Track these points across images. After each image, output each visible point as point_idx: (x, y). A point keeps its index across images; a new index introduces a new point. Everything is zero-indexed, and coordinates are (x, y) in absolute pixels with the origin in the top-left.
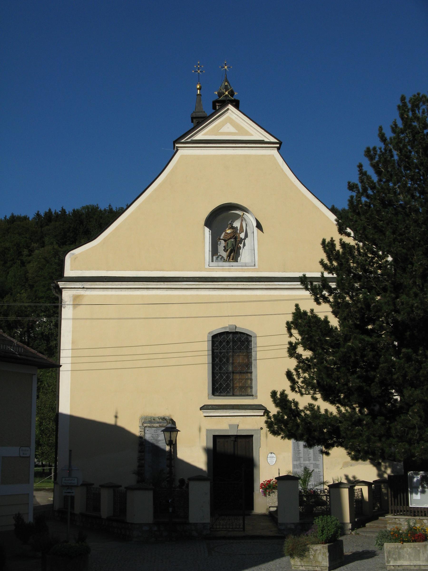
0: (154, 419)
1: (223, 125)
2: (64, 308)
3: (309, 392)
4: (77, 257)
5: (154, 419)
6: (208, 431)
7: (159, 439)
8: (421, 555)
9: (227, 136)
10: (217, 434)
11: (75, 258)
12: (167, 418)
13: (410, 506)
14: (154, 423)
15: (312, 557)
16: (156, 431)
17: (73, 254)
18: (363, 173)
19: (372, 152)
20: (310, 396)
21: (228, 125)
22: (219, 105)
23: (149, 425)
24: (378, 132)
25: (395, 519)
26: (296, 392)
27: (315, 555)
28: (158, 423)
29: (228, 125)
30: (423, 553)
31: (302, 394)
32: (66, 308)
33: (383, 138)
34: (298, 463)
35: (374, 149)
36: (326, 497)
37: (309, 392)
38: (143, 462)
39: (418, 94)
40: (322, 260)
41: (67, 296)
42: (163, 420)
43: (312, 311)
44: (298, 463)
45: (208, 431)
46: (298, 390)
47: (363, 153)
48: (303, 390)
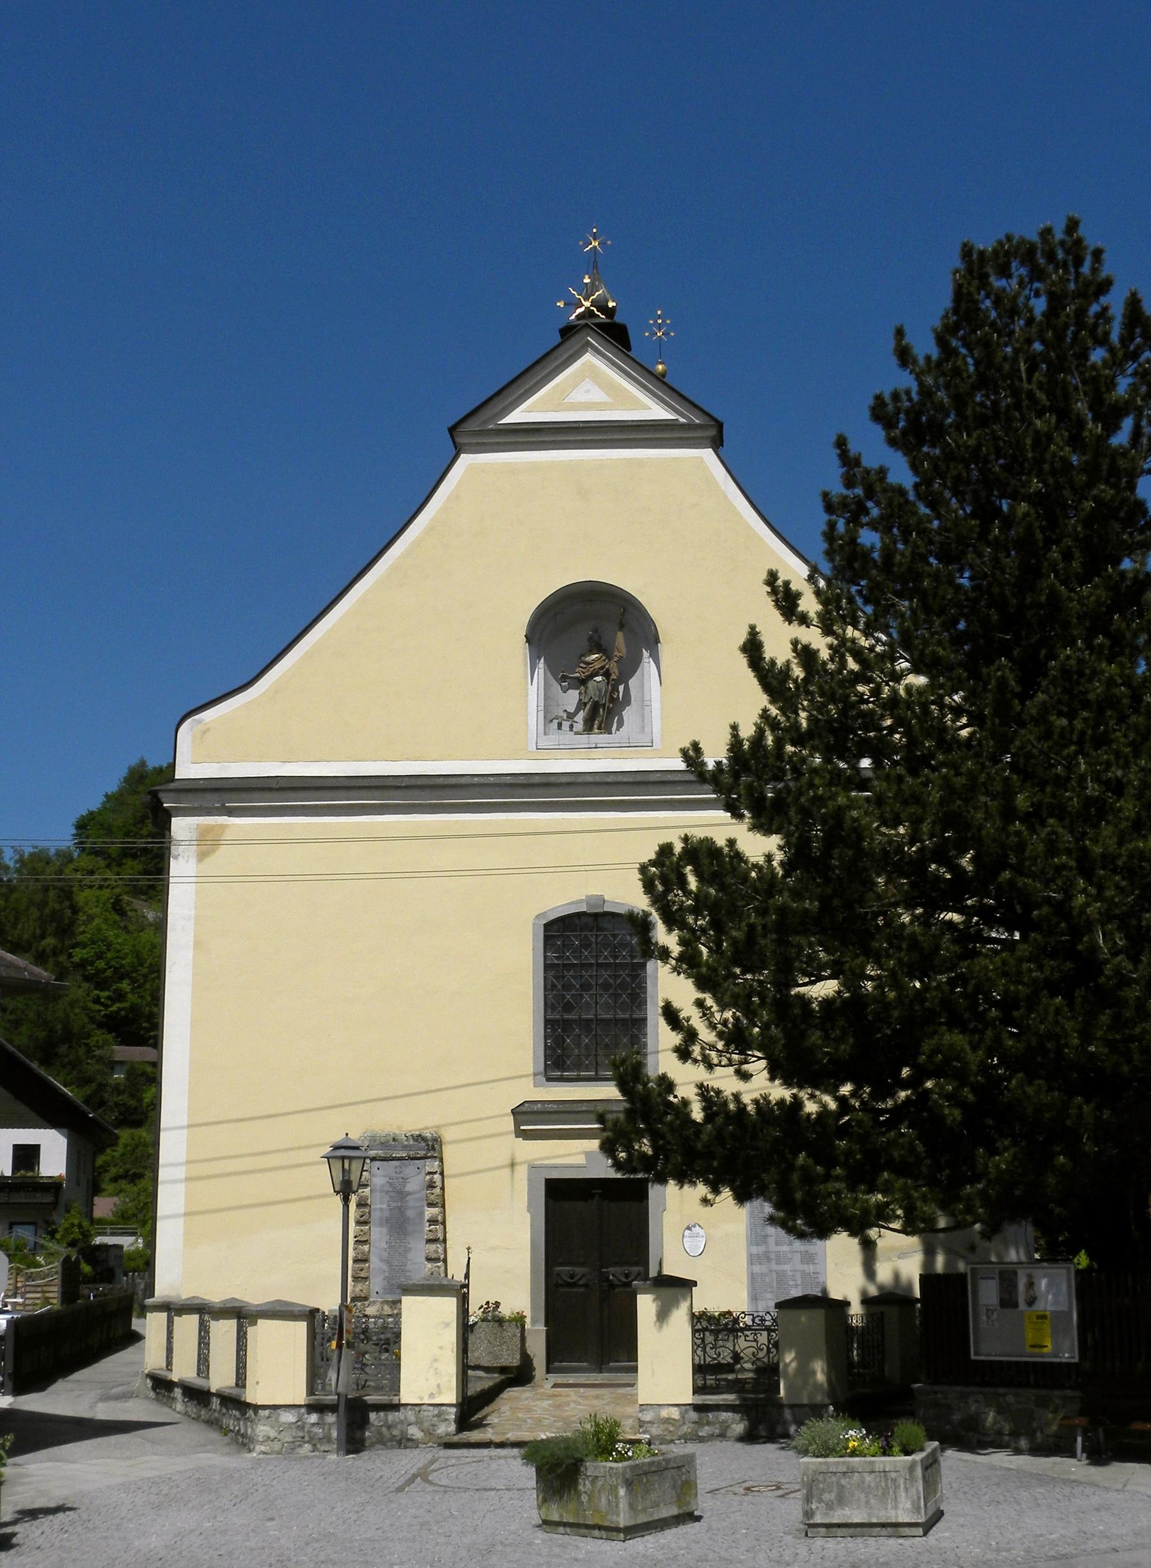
0: (394, 1140)
1: (575, 386)
2: (176, 858)
3: (729, 1060)
4: (208, 730)
5: (394, 1140)
6: (533, 1168)
7: (406, 1189)
8: (902, 1493)
9: (739, 508)
10: (555, 1175)
11: (205, 732)
12: (429, 1135)
13: (973, 1357)
14: (394, 1148)
15: (584, 1498)
16: (398, 1170)
17: (200, 722)
18: (848, 460)
19: (890, 408)
20: (731, 1069)
21: (587, 384)
22: (569, 338)
23: (381, 1153)
24: (892, 344)
25: (936, 1393)
26: (695, 1061)
27: (592, 1492)
28: (405, 1148)
29: (587, 384)
30: (906, 1489)
31: (710, 1066)
32: (180, 858)
33: (904, 355)
34: (761, 1249)
35: (896, 396)
36: (769, 1335)
37: (729, 1060)
38: (366, 1248)
39: (1009, 238)
40: (765, 711)
41: (181, 827)
42: (416, 1140)
43: (731, 843)
44: (761, 1249)
45: (533, 1168)
46: (699, 1058)
47: (867, 413)
48: (713, 1054)
